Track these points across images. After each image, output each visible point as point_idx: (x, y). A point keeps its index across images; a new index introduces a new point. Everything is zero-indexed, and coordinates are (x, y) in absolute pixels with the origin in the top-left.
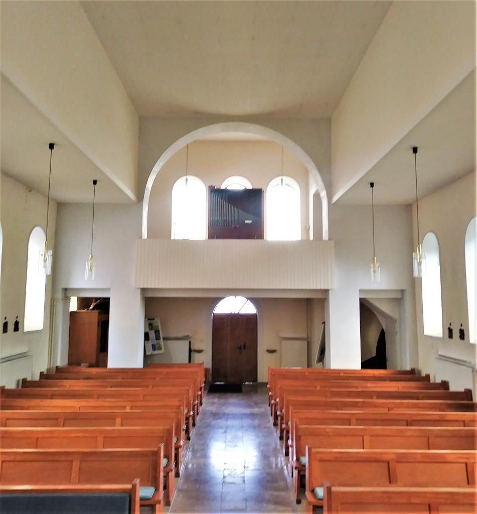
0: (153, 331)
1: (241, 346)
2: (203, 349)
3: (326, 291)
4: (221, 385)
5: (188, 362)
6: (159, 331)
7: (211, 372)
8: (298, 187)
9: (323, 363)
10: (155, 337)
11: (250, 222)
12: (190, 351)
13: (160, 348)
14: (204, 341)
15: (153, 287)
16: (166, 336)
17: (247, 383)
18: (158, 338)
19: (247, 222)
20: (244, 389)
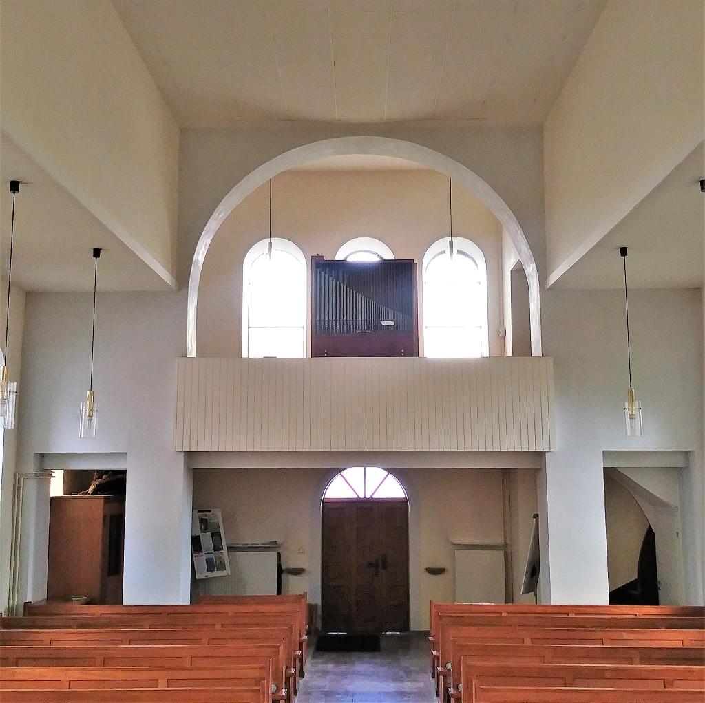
3: (540, 455)
5: (275, 593)
7: (320, 612)
12: (280, 571)
13: (222, 567)
14: (307, 553)
18: (217, 547)
19: (384, 323)
20: (383, 644)
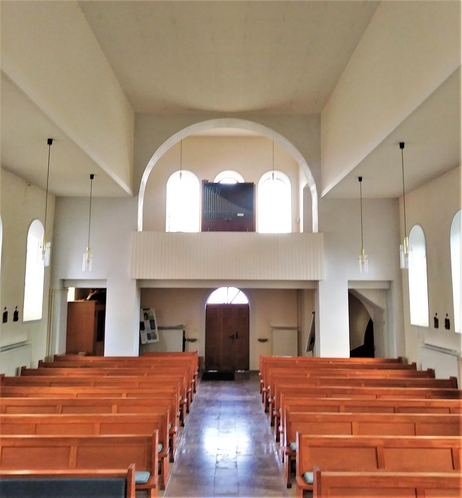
0: (149, 321)
1: (233, 335)
2: (196, 338)
3: (316, 282)
4: (215, 373)
5: (182, 351)
6: (154, 321)
7: (204, 361)
8: (289, 181)
9: (313, 352)
10: (150, 327)
11: (242, 215)
12: (184, 340)
13: (155, 338)
14: (198, 331)
15: (148, 278)
16: (161, 325)
17: (239, 371)
18: (153, 327)
19: (239, 215)
20: (236, 377)
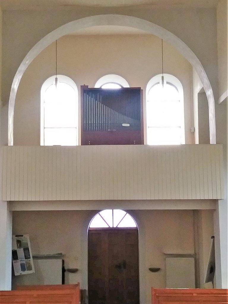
0: (22, 249)
3: (215, 202)
5: (61, 283)
6: (28, 249)
7: (87, 294)
12: (64, 270)
13: (30, 268)
14: (80, 260)
15: (17, 200)
16: (36, 254)
18: (27, 257)
19: (124, 125)
